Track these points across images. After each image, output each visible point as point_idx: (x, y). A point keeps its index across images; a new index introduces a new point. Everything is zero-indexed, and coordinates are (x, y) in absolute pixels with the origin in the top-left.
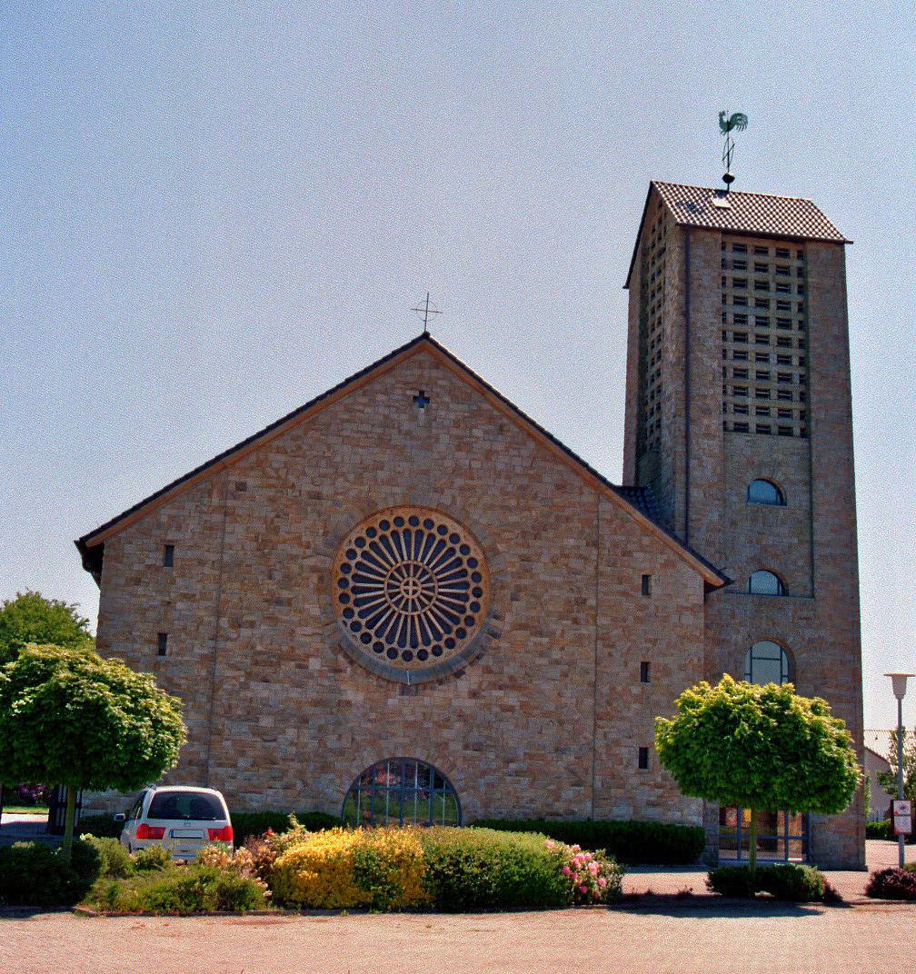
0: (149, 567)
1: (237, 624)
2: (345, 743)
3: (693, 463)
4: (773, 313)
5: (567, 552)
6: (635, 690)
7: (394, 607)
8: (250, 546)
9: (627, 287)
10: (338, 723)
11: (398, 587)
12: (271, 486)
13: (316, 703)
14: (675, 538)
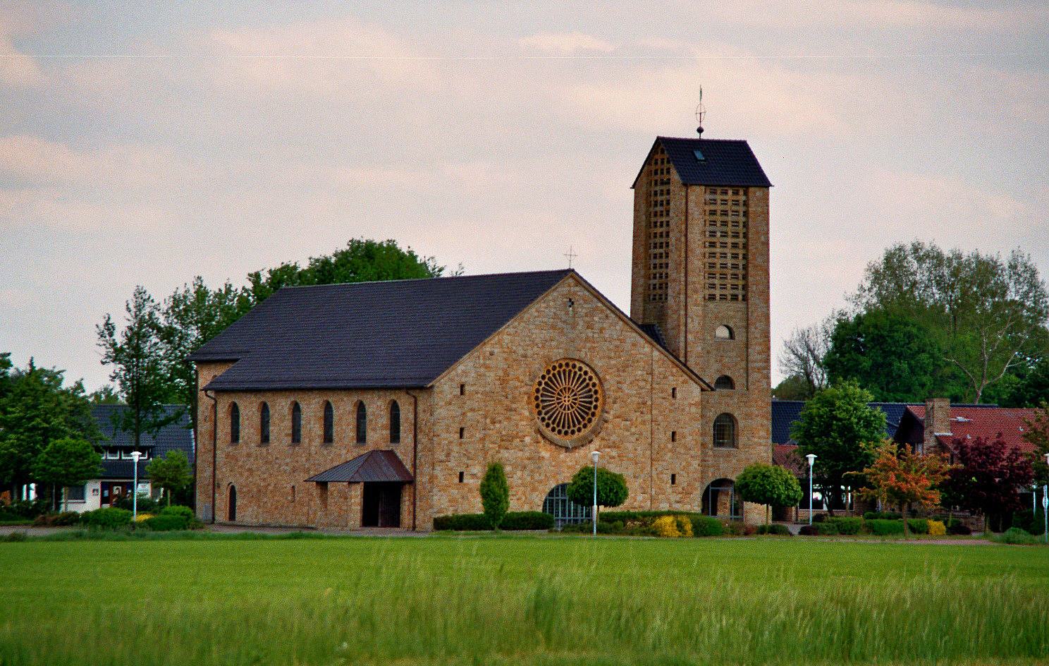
0: (454, 396)
1: (493, 422)
2: (543, 477)
3: (689, 320)
4: (730, 229)
5: (638, 378)
6: (670, 446)
7: (559, 409)
8: (498, 383)
9: (634, 187)
10: (539, 468)
12: (504, 352)
13: (529, 459)
14: (680, 361)
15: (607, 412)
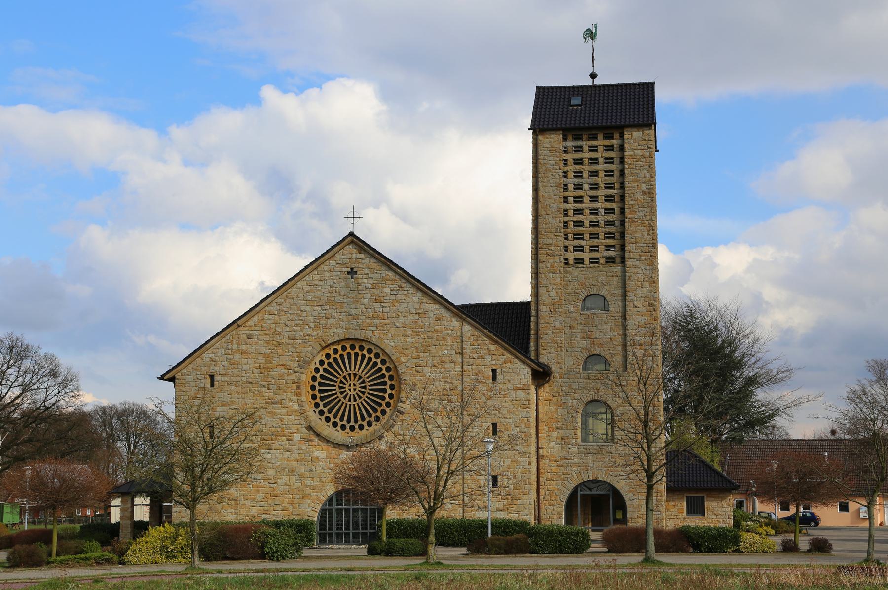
4: (601, 179)
11: (345, 388)
15: (401, 402)
